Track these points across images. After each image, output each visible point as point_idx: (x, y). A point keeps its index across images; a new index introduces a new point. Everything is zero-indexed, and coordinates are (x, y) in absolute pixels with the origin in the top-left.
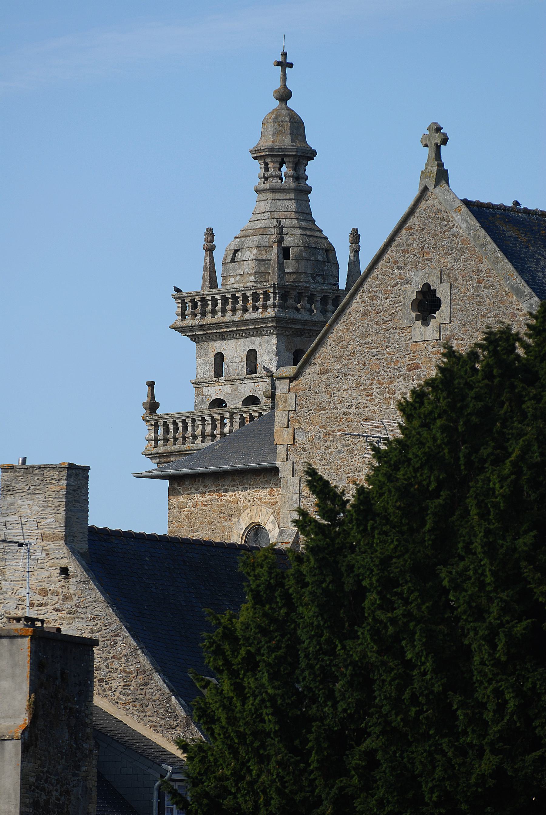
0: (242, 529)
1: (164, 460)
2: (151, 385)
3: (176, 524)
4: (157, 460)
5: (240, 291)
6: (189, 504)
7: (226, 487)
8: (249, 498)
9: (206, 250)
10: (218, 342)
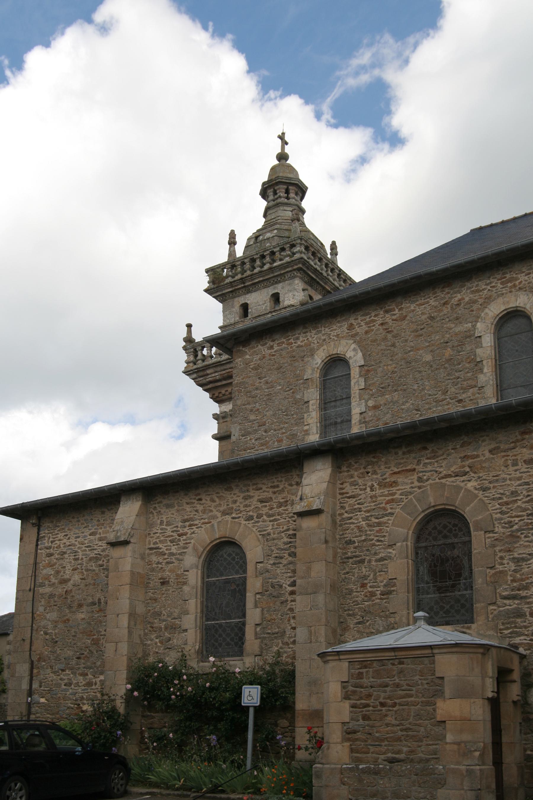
0: (317, 364)
1: (201, 374)
2: (189, 326)
3: (242, 377)
4: (195, 376)
5: (268, 250)
6: (255, 359)
7: (297, 335)
8: (323, 338)
9: (229, 244)
10: (242, 297)
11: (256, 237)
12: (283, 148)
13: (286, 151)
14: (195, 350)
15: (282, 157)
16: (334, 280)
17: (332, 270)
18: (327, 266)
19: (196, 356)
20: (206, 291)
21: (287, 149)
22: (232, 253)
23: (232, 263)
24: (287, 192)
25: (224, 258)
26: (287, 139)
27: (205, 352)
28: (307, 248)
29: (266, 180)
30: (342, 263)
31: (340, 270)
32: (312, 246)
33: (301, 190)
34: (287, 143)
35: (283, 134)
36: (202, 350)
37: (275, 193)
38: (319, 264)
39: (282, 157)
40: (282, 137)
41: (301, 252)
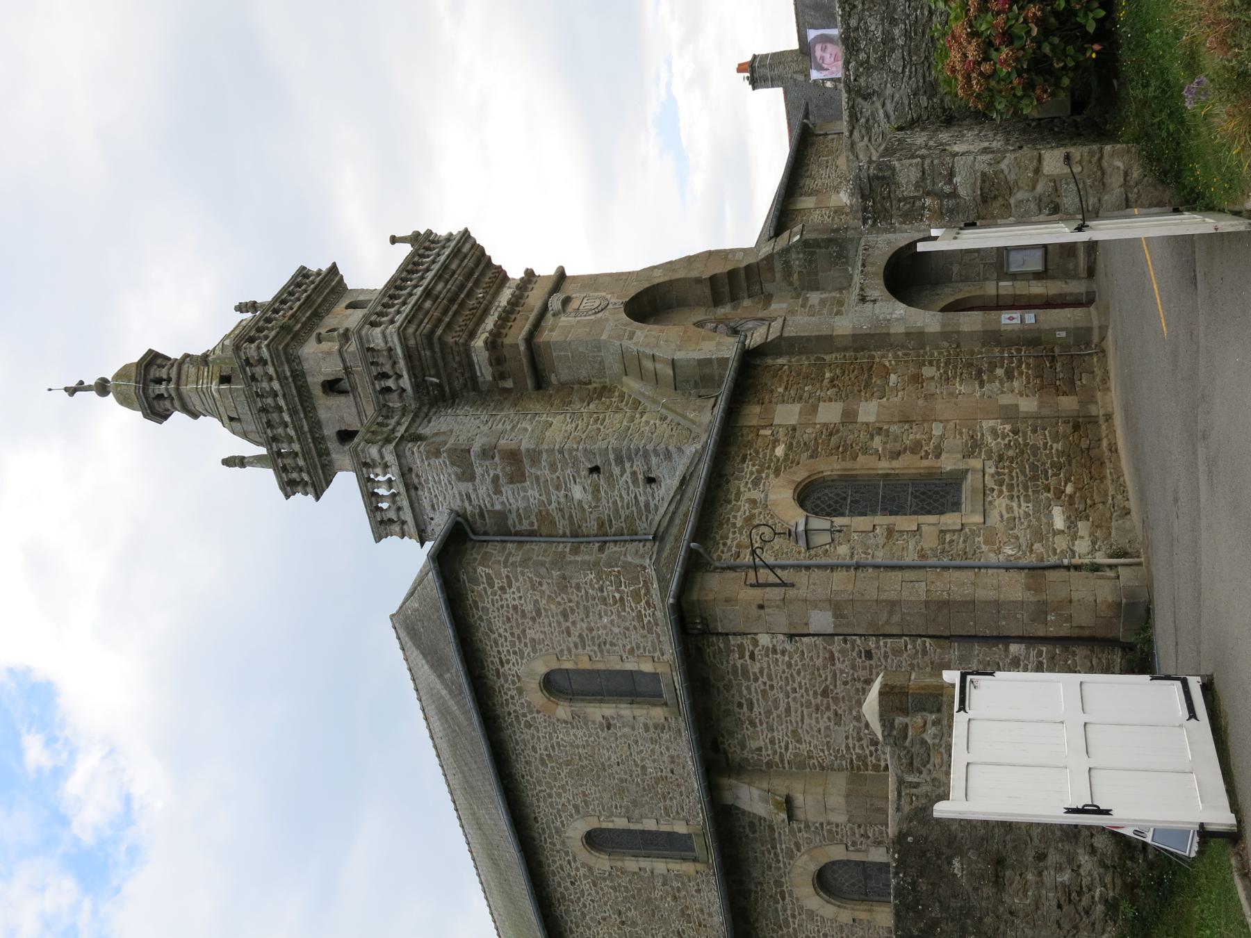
11: (232, 421)
12: (89, 388)
13: (93, 383)
14: (382, 522)
15: (102, 387)
16: (305, 291)
17: (276, 311)
18: (268, 320)
19: (391, 521)
20: (318, 498)
21: (90, 381)
22: (258, 461)
23: (274, 460)
24: (159, 381)
25: (267, 477)
26: (73, 384)
27: (385, 505)
28: (252, 340)
29: (140, 413)
30: (266, 295)
31: (276, 299)
32: (242, 338)
33: (153, 359)
34: (81, 383)
35: (66, 389)
36: (381, 509)
37: (160, 397)
38: (266, 332)
39: (102, 387)
40: (71, 391)
41: (259, 348)
